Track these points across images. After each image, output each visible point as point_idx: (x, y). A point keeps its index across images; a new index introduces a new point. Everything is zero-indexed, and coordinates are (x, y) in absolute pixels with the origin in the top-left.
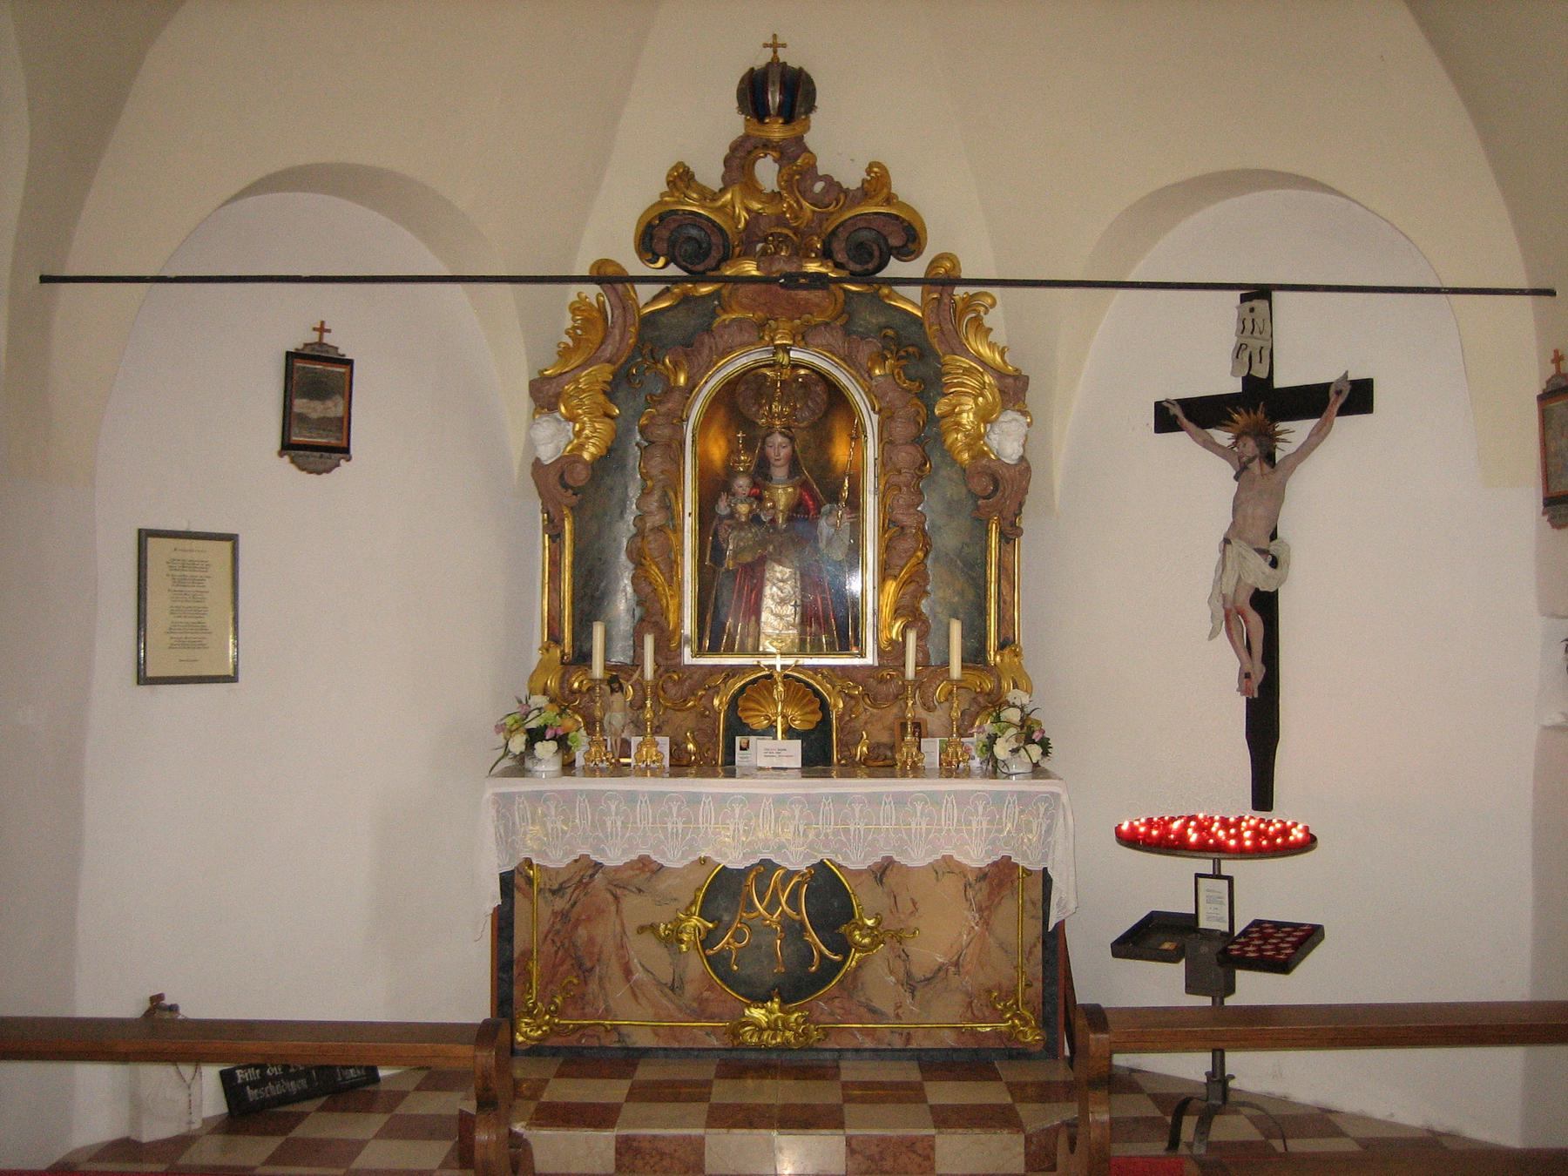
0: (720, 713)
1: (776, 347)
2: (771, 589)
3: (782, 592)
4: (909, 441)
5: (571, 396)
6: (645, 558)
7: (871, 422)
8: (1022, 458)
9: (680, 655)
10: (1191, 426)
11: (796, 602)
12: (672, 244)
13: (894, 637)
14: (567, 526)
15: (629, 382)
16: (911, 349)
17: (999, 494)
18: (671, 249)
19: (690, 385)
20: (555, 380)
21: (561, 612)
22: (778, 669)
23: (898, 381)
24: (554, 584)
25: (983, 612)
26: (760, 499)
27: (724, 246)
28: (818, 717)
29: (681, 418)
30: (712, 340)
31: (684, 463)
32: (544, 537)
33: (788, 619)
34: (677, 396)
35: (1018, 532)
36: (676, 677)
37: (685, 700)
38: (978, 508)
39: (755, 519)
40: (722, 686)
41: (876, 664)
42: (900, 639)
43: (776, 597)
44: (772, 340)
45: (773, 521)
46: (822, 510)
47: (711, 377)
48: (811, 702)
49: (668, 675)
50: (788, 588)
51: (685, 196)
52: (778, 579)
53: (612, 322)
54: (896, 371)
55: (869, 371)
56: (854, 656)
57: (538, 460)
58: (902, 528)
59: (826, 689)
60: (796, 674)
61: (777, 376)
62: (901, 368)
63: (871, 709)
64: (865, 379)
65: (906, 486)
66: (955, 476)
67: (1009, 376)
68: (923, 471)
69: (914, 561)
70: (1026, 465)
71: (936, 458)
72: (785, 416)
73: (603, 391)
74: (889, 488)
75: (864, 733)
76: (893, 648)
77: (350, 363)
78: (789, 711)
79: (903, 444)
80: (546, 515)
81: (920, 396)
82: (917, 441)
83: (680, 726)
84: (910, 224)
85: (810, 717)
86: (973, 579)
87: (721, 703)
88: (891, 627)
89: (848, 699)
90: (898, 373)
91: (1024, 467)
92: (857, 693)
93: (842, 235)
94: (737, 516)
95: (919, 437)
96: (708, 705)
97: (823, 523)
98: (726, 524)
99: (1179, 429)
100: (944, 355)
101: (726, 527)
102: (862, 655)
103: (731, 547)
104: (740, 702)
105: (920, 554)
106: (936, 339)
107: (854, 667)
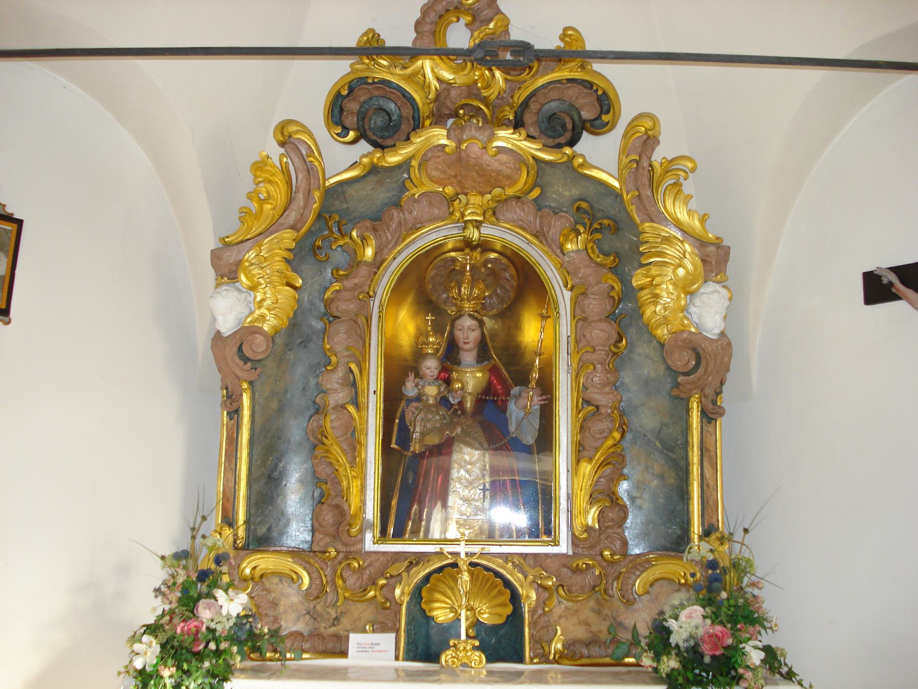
0: (401, 605)
1: (466, 222)
2: (458, 472)
3: (470, 475)
4: (603, 317)
5: (252, 264)
6: (326, 437)
7: (564, 298)
8: (722, 334)
9: (362, 541)
10: (909, 292)
11: (484, 486)
12: (362, 116)
13: (590, 523)
14: (246, 400)
15: (315, 254)
16: (606, 222)
17: (701, 370)
18: (361, 123)
19: (379, 259)
20: (236, 247)
21: (235, 491)
22: (463, 556)
23: (592, 256)
24: (229, 465)
25: (684, 495)
26: (448, 382)
27: (413, 118)
28: (509, 610)
29: (368, 293)
30: (401, 215)
31: (370, 340)
32: (223, 413)
33: (477, 504)
34: (363, 271)
35: (721, 412)
36: (356, 565)
37: (365, 590)
38: (677, 385)
39: (443, 401)
40: (405, 575)
41: (570, 553)
42: (597, 526)
43: (463, 481)
44: (463, 215)
45: (461, 404)
46: (512, 392)
47: (400, 252)
48: (500, 593)
49: (347, 562)
50: (476, 471)
51: (375, 63)
52: (465, 461)
53: (296, 187)
54: (590, 246)
55: (561, 248)
56: (547, 544)
57: (218, 332)
58: (597, 407)
59: (519, 580)
60: (485, 563)
61: (466, 260)
62: (594, 242)
63: (565, 602)
64: (557, 255)
65: (601, 364)
66: (652, 354)
67: (711, 244)
68: (618, 348)
69: (610, 442)
70: (728, 341)
71: (632, 332)
72: (475, 299)
73: (285, 259)
74: (582, 366)
75: (558, 628)
76: (589, 535)
77: (20, 223)
78: (476, 604)
79: (596, 321)
80: (225, 391)
81: (614, 270)
82: (612, 317)
83: (359, 618)
84: (604, 93)
85: (499, 610)
86: (674, 461)
87: (403, 593)
88: (587, 512)
89: (540, 590)
90: (592, 248)
91: (724, 343)
92: (550, 583)
93: (534, 106)
94: (424, 398)
95: (614, 312)
96: (389, 597)
97: (512, 407)
98: (413, 406)
99: (896, 297)
100: (643, 222)
101: (413, 409)
102: (556, 543)
103: (418, 429)
104: (424, 594)
105: (617, 435)
106: (634, 206)
107: (547, 555)
